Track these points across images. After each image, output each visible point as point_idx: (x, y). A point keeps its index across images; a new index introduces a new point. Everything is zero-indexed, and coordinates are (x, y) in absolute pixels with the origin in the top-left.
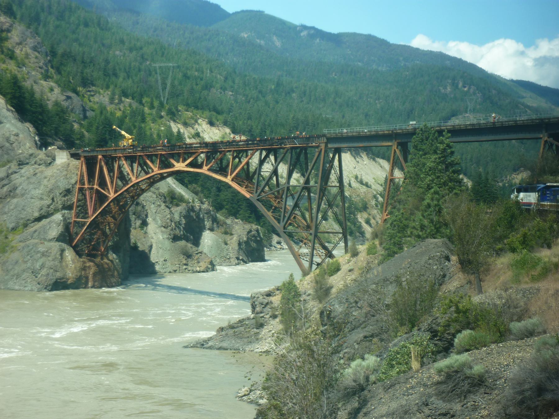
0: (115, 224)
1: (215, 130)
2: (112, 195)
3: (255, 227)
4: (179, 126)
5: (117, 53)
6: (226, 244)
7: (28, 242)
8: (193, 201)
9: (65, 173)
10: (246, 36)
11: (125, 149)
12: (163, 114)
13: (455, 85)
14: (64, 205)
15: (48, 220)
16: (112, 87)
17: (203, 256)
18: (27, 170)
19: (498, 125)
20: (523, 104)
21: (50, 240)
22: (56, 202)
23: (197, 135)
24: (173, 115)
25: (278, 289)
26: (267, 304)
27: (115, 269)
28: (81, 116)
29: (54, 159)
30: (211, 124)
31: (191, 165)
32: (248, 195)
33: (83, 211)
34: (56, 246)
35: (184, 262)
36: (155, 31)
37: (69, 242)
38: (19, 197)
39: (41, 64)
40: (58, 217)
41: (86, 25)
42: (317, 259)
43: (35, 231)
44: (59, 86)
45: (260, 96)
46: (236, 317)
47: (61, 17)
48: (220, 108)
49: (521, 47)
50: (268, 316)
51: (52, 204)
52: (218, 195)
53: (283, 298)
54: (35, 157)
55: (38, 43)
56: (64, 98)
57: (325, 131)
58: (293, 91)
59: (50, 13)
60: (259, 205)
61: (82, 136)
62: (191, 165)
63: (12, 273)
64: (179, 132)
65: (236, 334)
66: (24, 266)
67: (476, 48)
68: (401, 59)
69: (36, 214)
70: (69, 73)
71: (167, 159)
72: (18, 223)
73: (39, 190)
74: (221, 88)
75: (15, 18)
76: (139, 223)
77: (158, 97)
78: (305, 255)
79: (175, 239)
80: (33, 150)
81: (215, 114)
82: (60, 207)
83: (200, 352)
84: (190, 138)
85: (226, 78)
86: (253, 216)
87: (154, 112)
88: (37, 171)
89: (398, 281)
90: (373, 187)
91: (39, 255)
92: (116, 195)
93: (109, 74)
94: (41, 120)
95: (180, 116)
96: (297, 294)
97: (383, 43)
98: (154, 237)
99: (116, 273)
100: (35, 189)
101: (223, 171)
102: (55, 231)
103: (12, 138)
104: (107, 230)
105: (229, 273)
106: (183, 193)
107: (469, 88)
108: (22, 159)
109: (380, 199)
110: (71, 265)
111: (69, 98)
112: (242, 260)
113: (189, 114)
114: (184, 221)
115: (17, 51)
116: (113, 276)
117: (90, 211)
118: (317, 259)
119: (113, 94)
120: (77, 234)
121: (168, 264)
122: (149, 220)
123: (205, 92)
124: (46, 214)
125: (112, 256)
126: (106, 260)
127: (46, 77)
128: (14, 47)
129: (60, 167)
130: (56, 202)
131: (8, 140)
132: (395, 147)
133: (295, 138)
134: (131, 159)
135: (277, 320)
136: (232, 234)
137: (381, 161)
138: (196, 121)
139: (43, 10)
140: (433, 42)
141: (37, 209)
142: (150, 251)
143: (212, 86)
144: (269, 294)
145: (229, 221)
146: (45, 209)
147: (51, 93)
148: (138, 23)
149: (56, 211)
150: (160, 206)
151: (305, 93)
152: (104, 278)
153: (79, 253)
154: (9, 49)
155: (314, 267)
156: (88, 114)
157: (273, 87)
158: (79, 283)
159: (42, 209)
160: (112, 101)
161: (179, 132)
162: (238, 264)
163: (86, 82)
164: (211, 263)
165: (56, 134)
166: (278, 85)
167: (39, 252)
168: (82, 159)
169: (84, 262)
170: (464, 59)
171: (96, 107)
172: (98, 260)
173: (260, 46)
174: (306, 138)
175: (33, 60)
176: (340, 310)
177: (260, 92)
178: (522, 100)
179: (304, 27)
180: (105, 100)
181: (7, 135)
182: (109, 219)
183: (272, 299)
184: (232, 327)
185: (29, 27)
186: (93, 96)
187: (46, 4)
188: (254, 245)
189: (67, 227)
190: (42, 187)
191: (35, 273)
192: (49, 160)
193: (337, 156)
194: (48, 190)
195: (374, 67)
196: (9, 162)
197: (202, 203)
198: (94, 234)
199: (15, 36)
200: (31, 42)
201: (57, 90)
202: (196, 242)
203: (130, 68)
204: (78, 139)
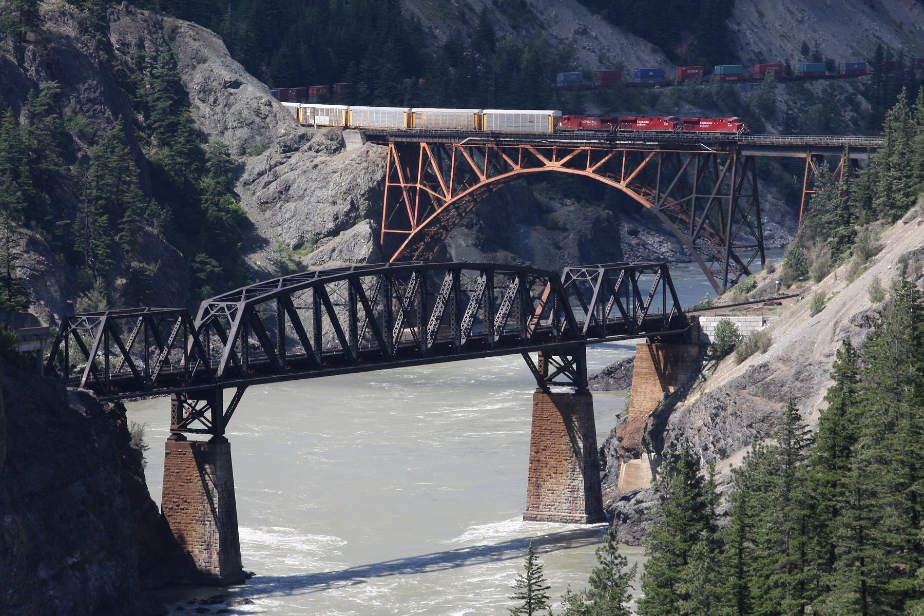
2: (449, 199)
6: (559, 248)
9: (364, 165)
38: (296, 200)
43: (334, 250)
60: (661, 216)
62: (564, 165)
69: (331, 225)
72: (302, 237)
78: (719, 272)
100: (321, 188)
103: (264, 110)
117: (413, 222)
129: (354, 156)
131: (258, 113)
132: (809, 160)
141: (331, 218)
146: (341, 217)
181: (254, 104)
190: (331, 186)
196: (265, 147)
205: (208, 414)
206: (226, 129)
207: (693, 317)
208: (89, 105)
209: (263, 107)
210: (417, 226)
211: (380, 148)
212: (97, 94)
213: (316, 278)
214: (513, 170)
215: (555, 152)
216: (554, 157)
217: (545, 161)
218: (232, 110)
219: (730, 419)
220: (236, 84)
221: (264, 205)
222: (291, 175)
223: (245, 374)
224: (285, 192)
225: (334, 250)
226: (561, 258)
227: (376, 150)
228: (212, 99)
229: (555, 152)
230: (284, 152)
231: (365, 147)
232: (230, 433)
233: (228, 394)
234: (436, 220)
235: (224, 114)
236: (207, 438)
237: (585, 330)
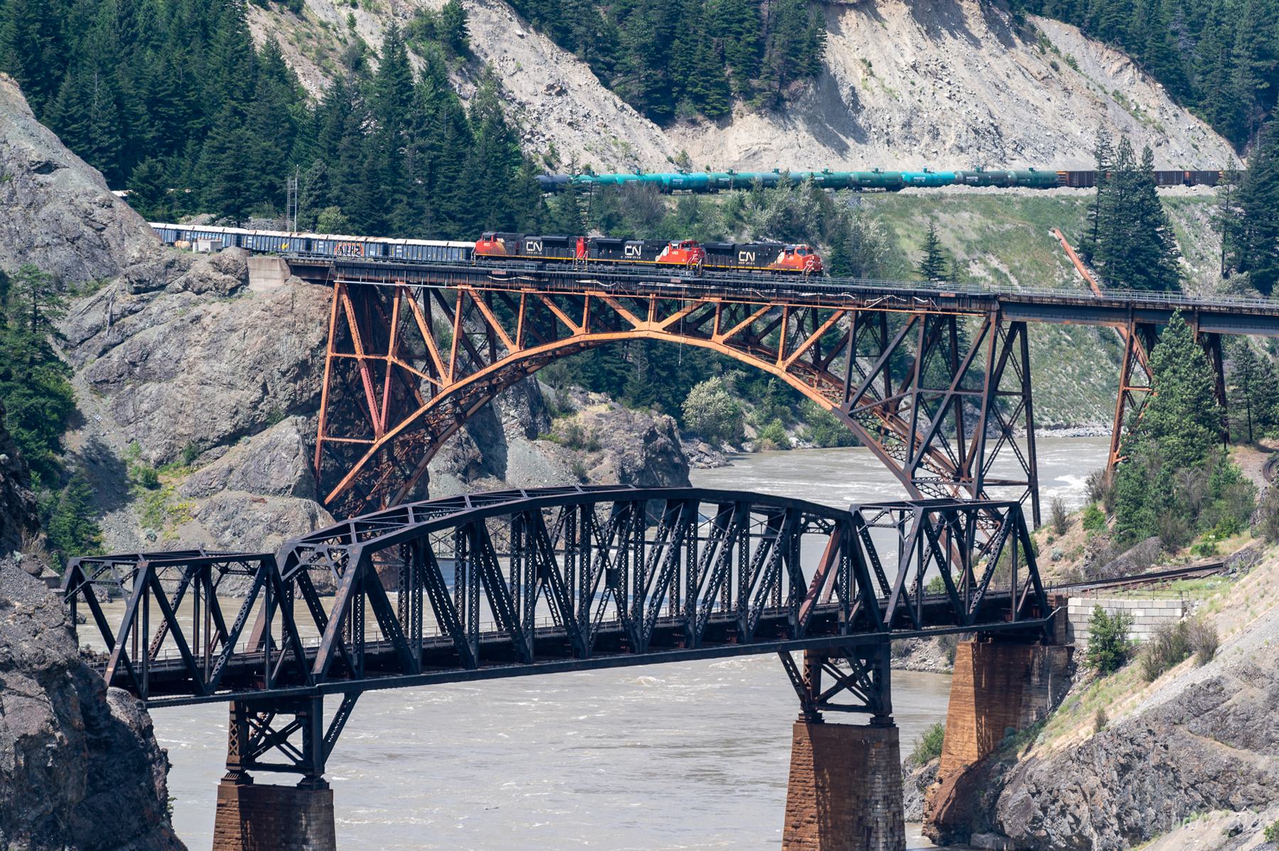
14: (294, 401)
21: (279, 492)
22: (271, 393)
29: (246, 281)
43: (231, 471)
51: (262, 399)
54: (183, 271)
62: (670, 329)
69: (226, 426)
72: (171, 447)
73: (220, 361)
82: (284, 405)
92: (461, 383)
103: (100, 214)
108: (146, 277)
117: (378, 423)
124: (247, 426)
130: (271, 393)
131: (87, 216)
137: (1051, 28)
141: (226, 413)
159: (236, 413)
167: (257, 521)
194: (248, 362)
205: (297, 739)
207: (1059, 598)
210: (387, 431)
211: (317, 290)
213: (469, 508)
214: (570, 333)
215: (652, 306)
216: (651, 314)
217: (635, 321)
218: (42, 215)
219: (1152, 774)
220: (48, 167)
222: (151, 335)
223: (359, 670)
225: (231, 471)
227: (311, 297)
229: (652, 306)
230: (138, 291)
231: (286, 292)
232: (333, 773)
233: (331, 703)
234: (421, 422)
235: (27, 220)
236: (864, 719)
237: (889, 614)
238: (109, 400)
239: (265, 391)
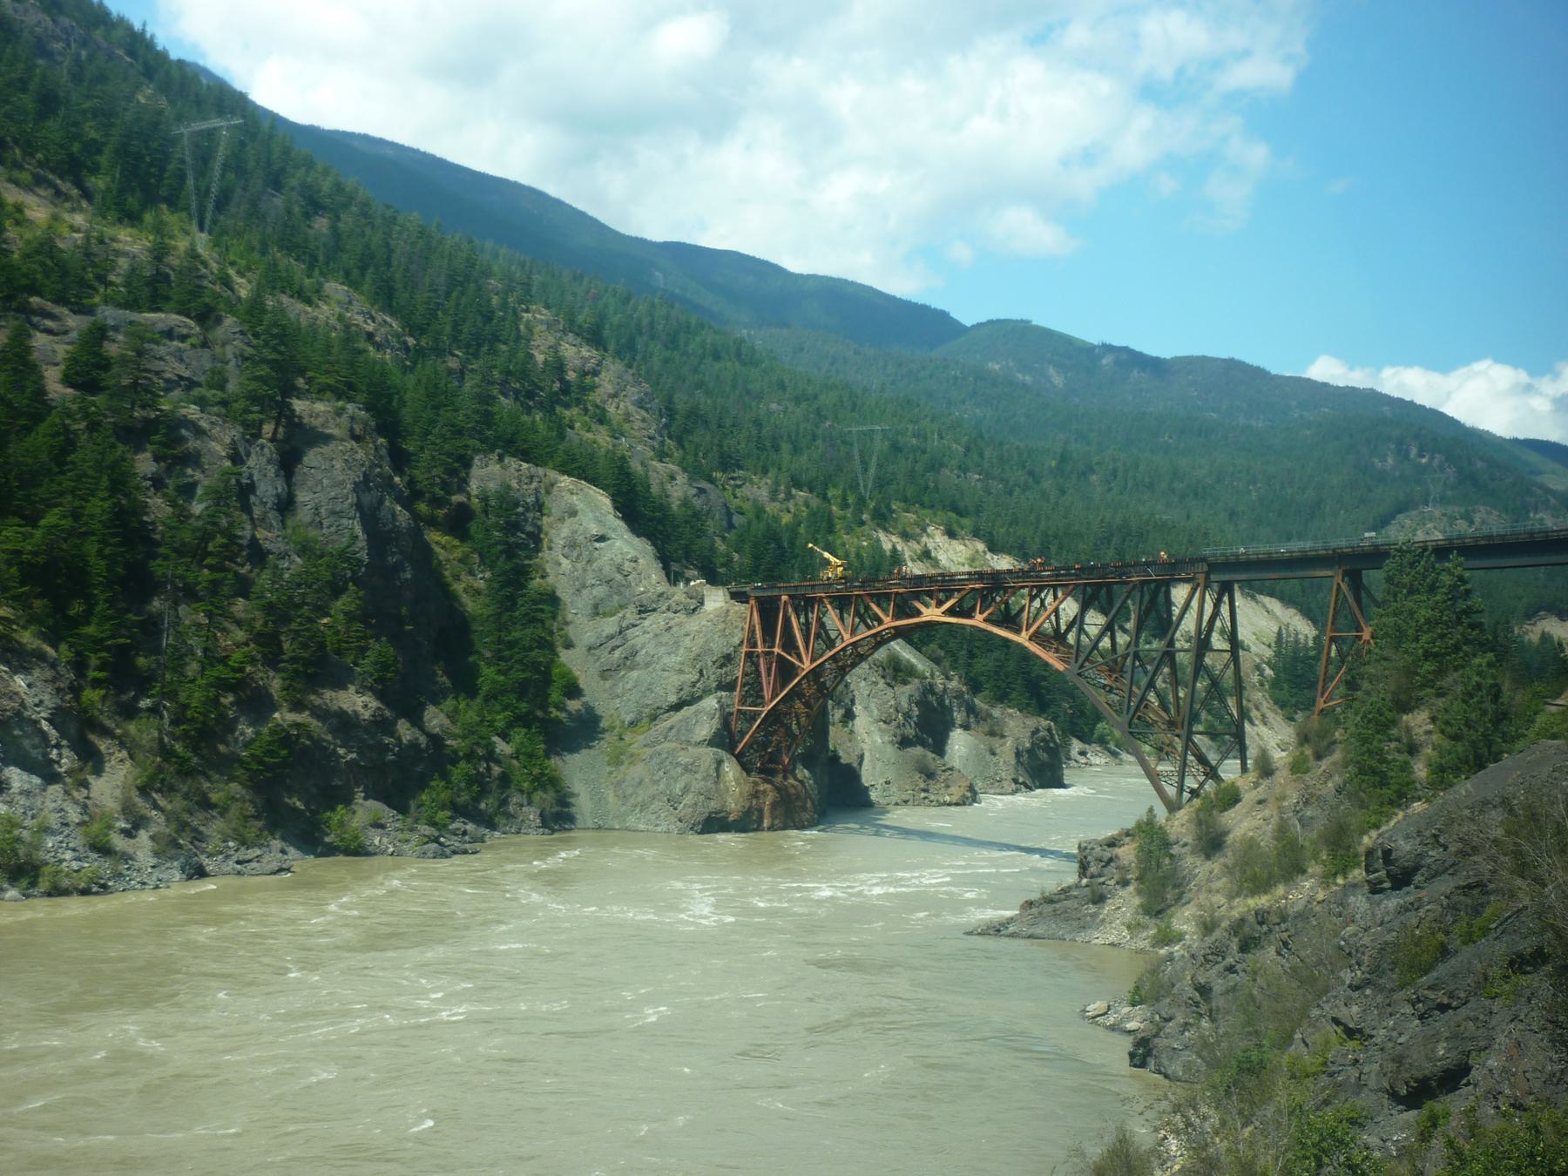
0: (808, 716)
1: (957, 546)
2: (807, 666)
3: (1044, 723)
4: (894, 538)
5: (774, 406)
6: (994, 754)
7: (658, 748)
8: (932, 675)
10: (997, 367)
11: (830, 585)
12: (865, 517)
13: (1402, 453)
15: (693, 708)
16: (772, 472)
17: (955, 774)
18: (653, 622)
19: (1538, 537)
20: (1542, 487)
23: (926, 555)
24: (883, 519)
25: (1127, 835)
26: (1111, 860)
27: (808, 796)
28: (724, 523)
29: (702, 603)
30: (951, 534)
31: (951, 612)
32: (1060, 666)
33: (753, 693)
34: (708, 754)
35: (923, 786)
36: (832, 364)
37: (730, 749)
39: (652, 431)
40: (710, 703)
41: (717, 357)
42: (1191, 783)
43: (671, 728)
44: (685, 470)
45: (1030, 480)
46: (1052, 885)
47: (672, 342)
48: (961, 505)
49: (1523, 377)
50: (1112, 882)
52: (970, 665)
53: (1141, 849)
55: (646, 394)
56: (694, 491)
57: (1207, 552)
58: (1092, 471)
59: (652, 337)
61: (728, 563)
62: (951, 612)
63: (632, 801)
64: (894, 550)
65: (1054, 914)
66: (653, 790)
67: (1436, 378)
68: (1294, 403)
69: (673, 699)
70: (697, 446)
71: (906, 602)
72: (640, 713)
74: (959, 468)
75: (606, 350)
76: (838, 714)
77: (854, 486)
79: (904, 743)
80: (663, 587)
81: (953, 515)
83: (990, 943)
84: (913, 560)
85: (968, 449)
86: (1034, 702)
87: (849, 513)
88: (672, 623)
89: (1505, 803)
90: (1253, 648)
91: (679, 770)
93: (766, 449)
94: (661, 532)
95: (896, 520)
96: (1166, 844)
97: (1258, 373)
98: (868, 736)
99: (809, 804)
101: (1010, 620)
102: (706, 729)
103: (627, 566)
104: (794, 727)
105: (1008, 807)
106: (914, 661)
107: (1432, 459)
109: (1269, 672)
110: (734, 789)
111: (702, 491)
112: (1024, 783)
113: (912, 517)
114: (916, 711)
115: (611, 409)
116: (804, 808)
117: (767, 694)
118: (1191, 783)
119: (777, 483)
120: (743, 734)
121: (894, 789)
122: (857, 709)
123: (930, 476)
125: (803, 773)
126: (791, 781)
127: (662, 455)
128: (604, 402)
131: (619, 569)
133: (1148, 564)
134: (842, 603)
135: (1131, 888)
136: (1003, 736)
137: (1267, 600)
138: (924, 530)
139: (641, 334)
140: (1351, 369)
142: (860, 764)
143: (942, 465)
144: (1112, 843)
145: (996, 712)
146: (687, 689)
147: (674, 486)
148: (802, 349)
149: (707, 692)
150: (876, 683)
151: (1114, 473)
152: (791, 814)
153: (746, 767)
154: (597, 407)
155: (1186, 795)
156: (737, 520)
157: (1054, 463)
158: (746, 823)
160: (773, 498)
161: (894, 550)
162: (1014, 792)
163: (728, 463)
164: (971, 788)
165: (687, 556)
166: (1063, 459)
168: (752, 602)
169: (756, 784)
170: (1419, 401)
171: (747, 506)
172: (779, 779)
173: (1024, 385)
174: (1170, 564)
175: (637, 425)
176: (1408, 848)
177: (1031, 473)
178: (1539, 479)
179: (1108, 348)
180: (763, 494)
181: (618, 560)
182: (798, 705)
183: (1118, 851)
184: (1049, 901)
185: (630, 366)
186: (739, 486)
187: (645, 322)
188: (1044, 756)
189: (726, 720)
190: (682, 651)
191: (673, 801)
192: (693, 603)
193: (1226, 599)
194: (692, 656)
195: (1242, 420)
196: (622, 607)
197: (948, 678)
198: (772, 734)
199: (605, 383)
200: (633, 392)
201: (681, 478)
202: (939, 748)
203: (797, 434)
204: (723, 565)
206: (584, 587)
208: (332, 519)
209: (627, 564)
212: (346, 505)
217: (923, 609)
221: (605, 674)
222: (639, 641)
224: (629, 662)
226: (996, 764)
228: (575, 554)
235: (585, 570)
238: (608, 684)
239: (701, 674)
